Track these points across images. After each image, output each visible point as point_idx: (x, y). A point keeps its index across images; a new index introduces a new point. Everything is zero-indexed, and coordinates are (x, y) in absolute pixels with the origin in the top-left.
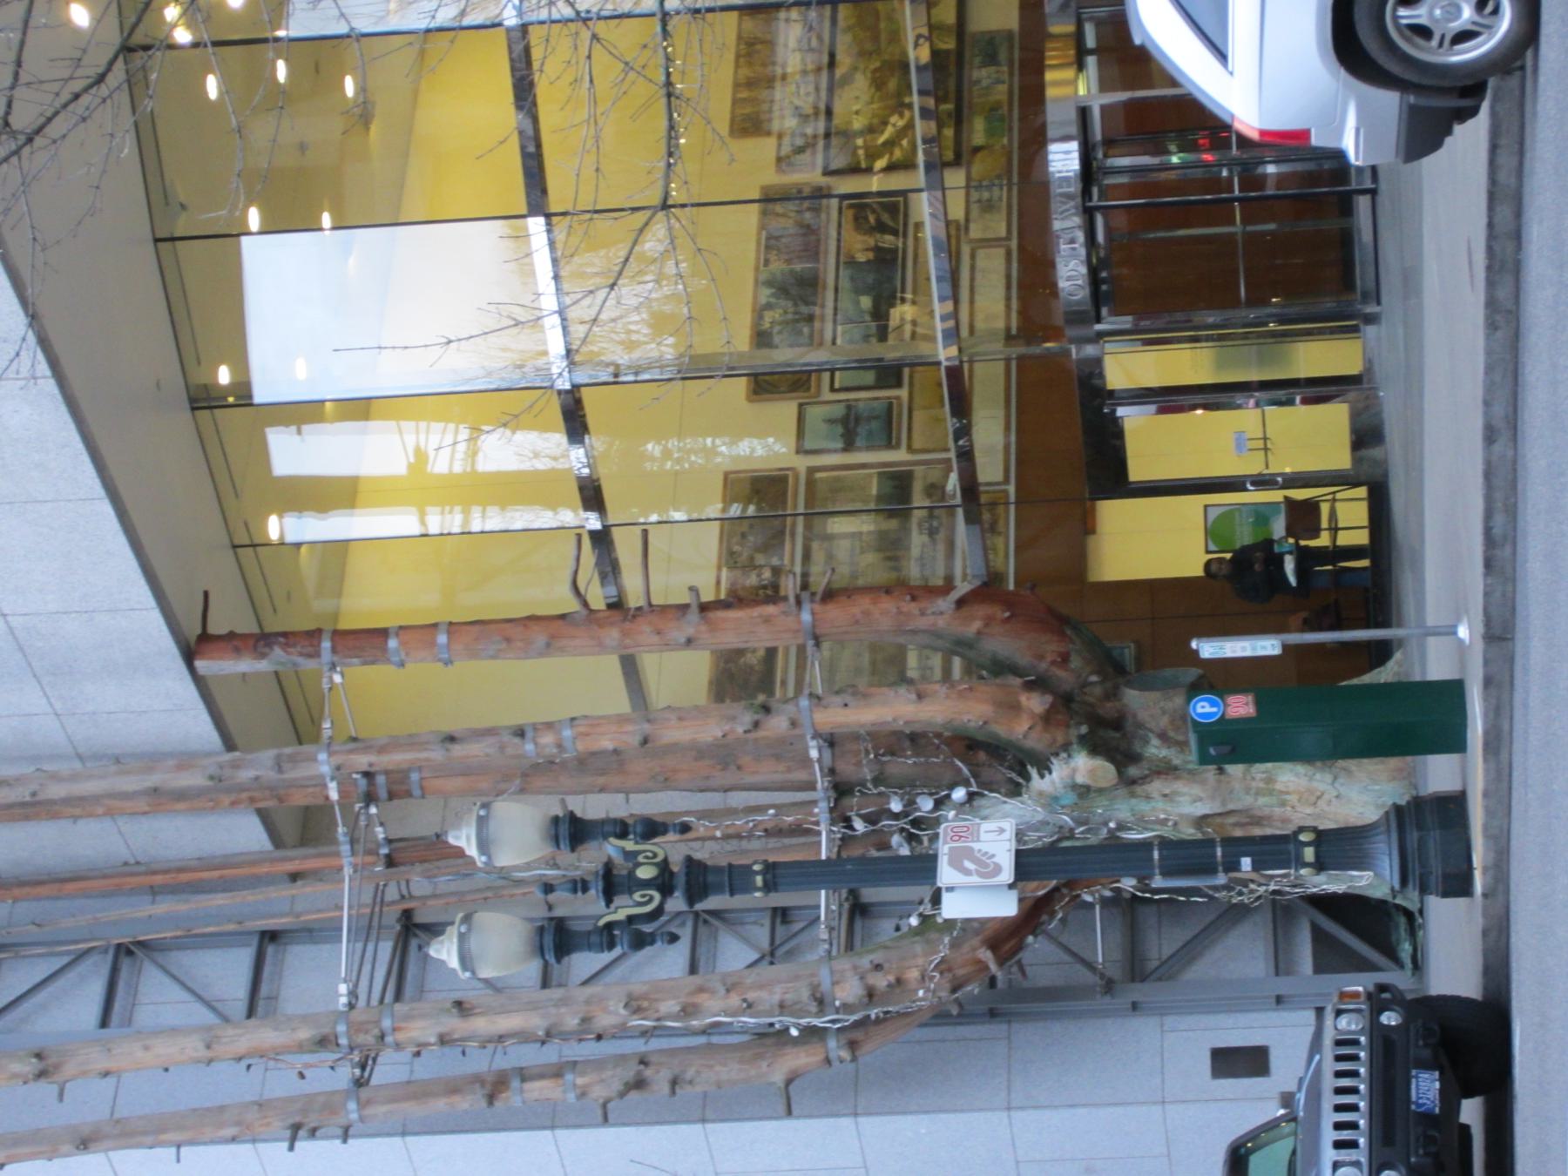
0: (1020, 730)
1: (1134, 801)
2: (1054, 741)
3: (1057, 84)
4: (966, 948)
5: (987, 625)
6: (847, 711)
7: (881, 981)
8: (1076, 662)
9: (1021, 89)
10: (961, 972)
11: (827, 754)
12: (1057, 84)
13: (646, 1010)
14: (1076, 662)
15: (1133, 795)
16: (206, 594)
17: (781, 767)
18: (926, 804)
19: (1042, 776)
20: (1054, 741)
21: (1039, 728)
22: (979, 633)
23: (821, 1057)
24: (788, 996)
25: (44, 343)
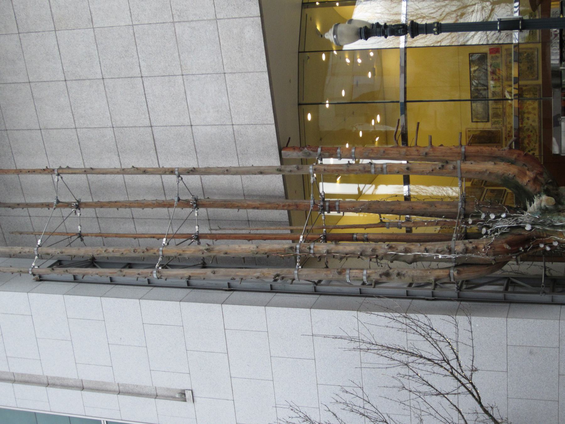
0: (525, 181)
1: (559, 217)
2: (536, 190)
3: (553, 5)
4: (500, 242)
5: (518, 156)
6: (471, 165)
7: (470, 246)
8: (545, 176)
9: (544, 119)
10: (497, 250)
11: (464, 204)
12: (553, 5)
13: (394, 248)
14: (545, 176)
15: (559, 215)
16: (290, 138)
17: (448, 207)
18: (492, 216)
19: (531, 205)
20: (536, 190)
21: (531, 182)
22: (516, 159)
23: (448, 274)
24: (440, 249)
25: (262, 16)
